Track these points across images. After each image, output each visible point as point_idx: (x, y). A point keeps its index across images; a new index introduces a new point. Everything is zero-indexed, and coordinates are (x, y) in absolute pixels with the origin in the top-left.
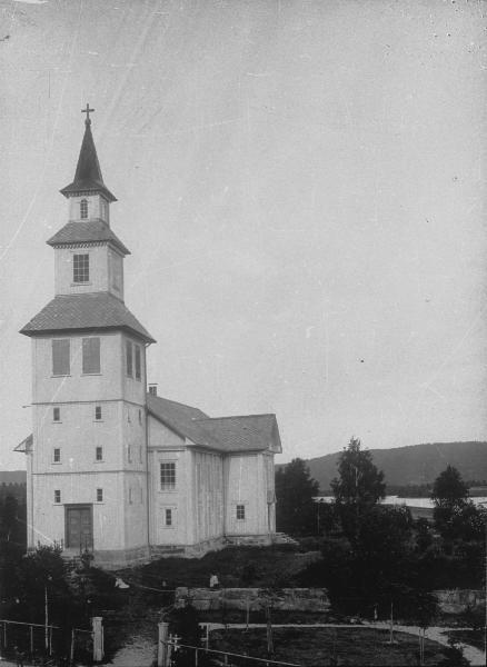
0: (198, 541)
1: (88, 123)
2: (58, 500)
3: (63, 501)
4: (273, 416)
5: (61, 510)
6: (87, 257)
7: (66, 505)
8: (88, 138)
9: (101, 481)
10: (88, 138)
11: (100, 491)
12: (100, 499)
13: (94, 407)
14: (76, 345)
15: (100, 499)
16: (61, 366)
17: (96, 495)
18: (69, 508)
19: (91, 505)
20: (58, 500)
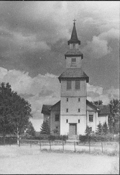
0: (22, 97)
1: (74, 24)
2: (67, 122)
3: (69, 122)
4: (44, 106)
5: (68, 125)
6: (75, 59)
7: (69, 123)
8: (74, 28)
9: (78, 118)
10: (74, 28)
11: (79, 120)
12: (79, 122)
13: (78, 98)
14: (73, 83)
15: (79, 122)
16: (69, 87)
17: (78, 121)
18: (71, 124)
19: (77, 123)
20: (67, 122)
